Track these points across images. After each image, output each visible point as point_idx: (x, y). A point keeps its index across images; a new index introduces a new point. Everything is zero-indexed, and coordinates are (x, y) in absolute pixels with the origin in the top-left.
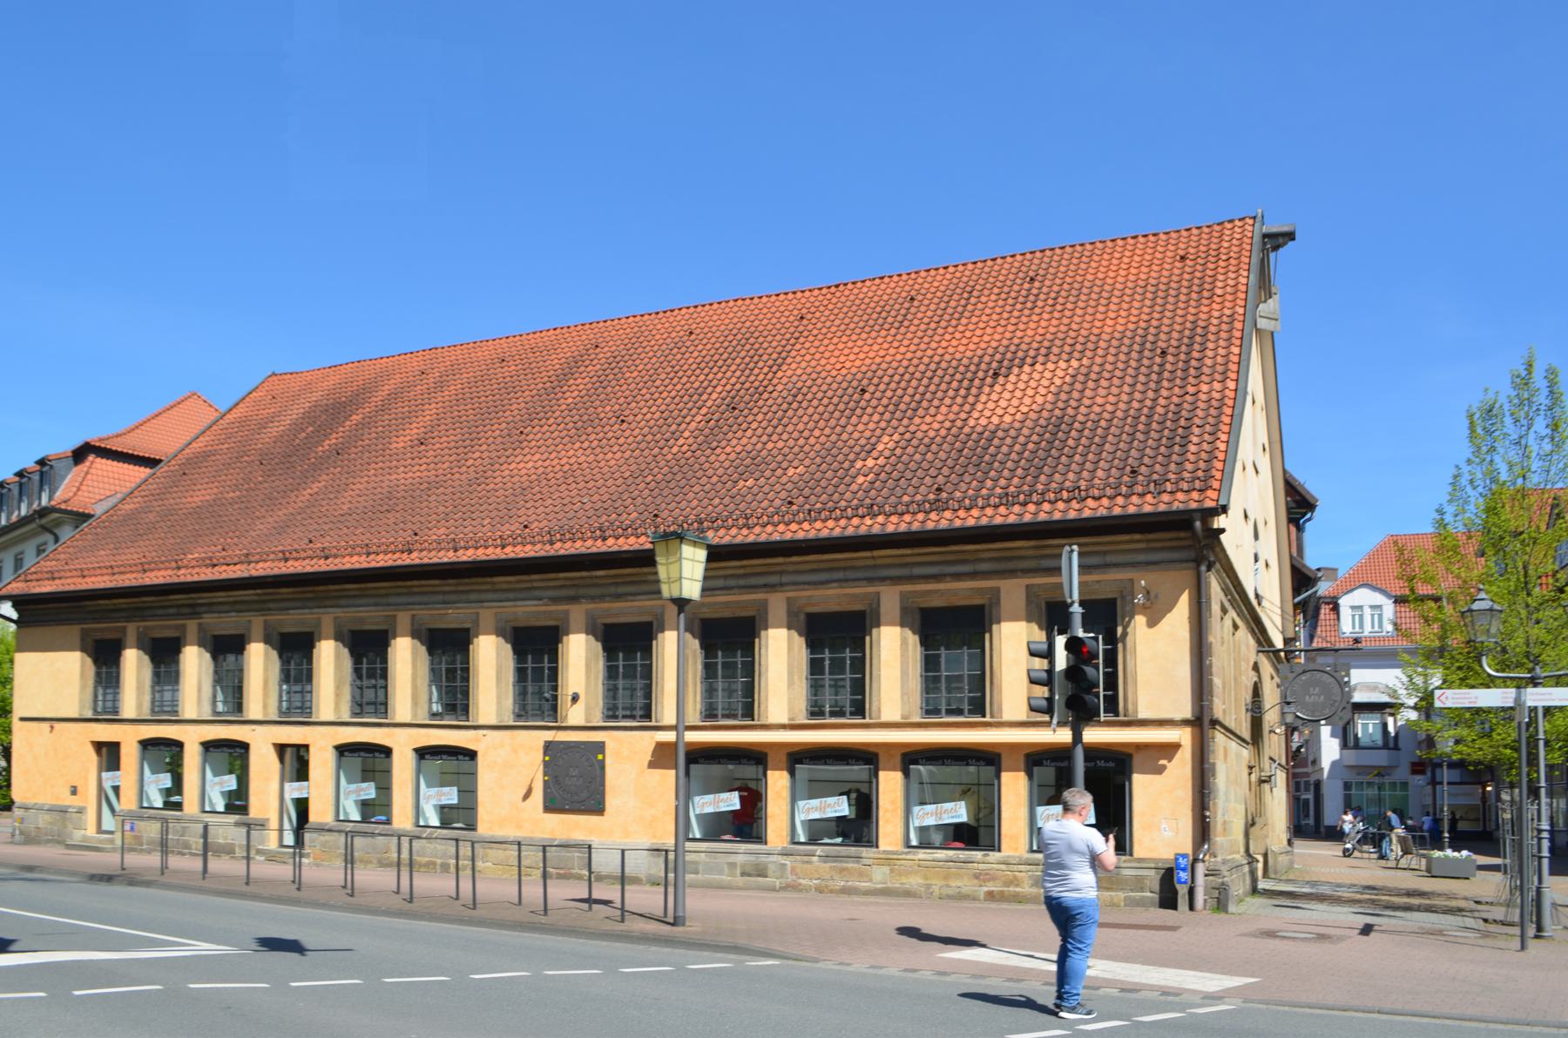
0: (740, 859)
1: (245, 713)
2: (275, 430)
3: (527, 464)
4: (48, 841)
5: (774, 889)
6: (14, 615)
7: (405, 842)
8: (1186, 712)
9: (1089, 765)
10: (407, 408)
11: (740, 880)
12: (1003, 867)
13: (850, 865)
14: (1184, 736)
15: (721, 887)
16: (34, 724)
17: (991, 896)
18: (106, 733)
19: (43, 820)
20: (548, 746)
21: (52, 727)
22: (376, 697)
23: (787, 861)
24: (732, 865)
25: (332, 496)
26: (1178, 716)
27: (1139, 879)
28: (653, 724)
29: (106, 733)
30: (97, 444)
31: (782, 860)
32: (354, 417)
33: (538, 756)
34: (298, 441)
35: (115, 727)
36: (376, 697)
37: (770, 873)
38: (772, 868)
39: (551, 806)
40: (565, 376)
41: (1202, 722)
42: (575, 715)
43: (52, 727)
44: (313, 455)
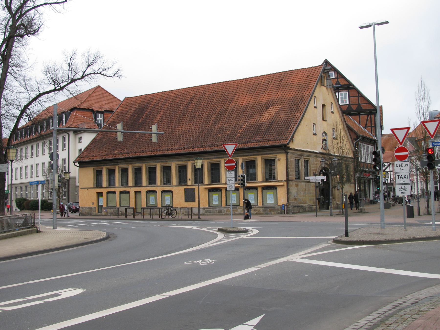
0: (218, 209)
1: (128, 185)
2: (129, 115)
3: (181, 128)
4: (88, 215)
5: (223, 215)
6: (78, 165)
7: (160, 210)
8: (285, 179)
9: (311, 175)
10: (157, 111)
11: (218, 213)
12: (258, 208)
13: (235, 209)
14: (286, 183)
15: (214, 215)
16: (84, 189)
17: (256, 213)
18: (99, 190)
19: (86, 211)
20: (185, 189)
21: (88, 190)
22: (194, 215)
23: (225, 209)
24: (216, 210)
25: (143, 136)
26: (283, 180)
27: (278, 209)
28: (203, 184)
29: (99, 190)
30: (77, 107)
31: (224, 209)
32: (146, 113)
33: (183, 192)
34: (134, 119)
35: (102, 189)
36: (194, 215)
37: (222, 212)
38: (223, 211)
39: (186, 201)
40: (190, 103)
41: (288, 181)
42: (190, 183)
43: (88, 190)
44: (138, 124)
